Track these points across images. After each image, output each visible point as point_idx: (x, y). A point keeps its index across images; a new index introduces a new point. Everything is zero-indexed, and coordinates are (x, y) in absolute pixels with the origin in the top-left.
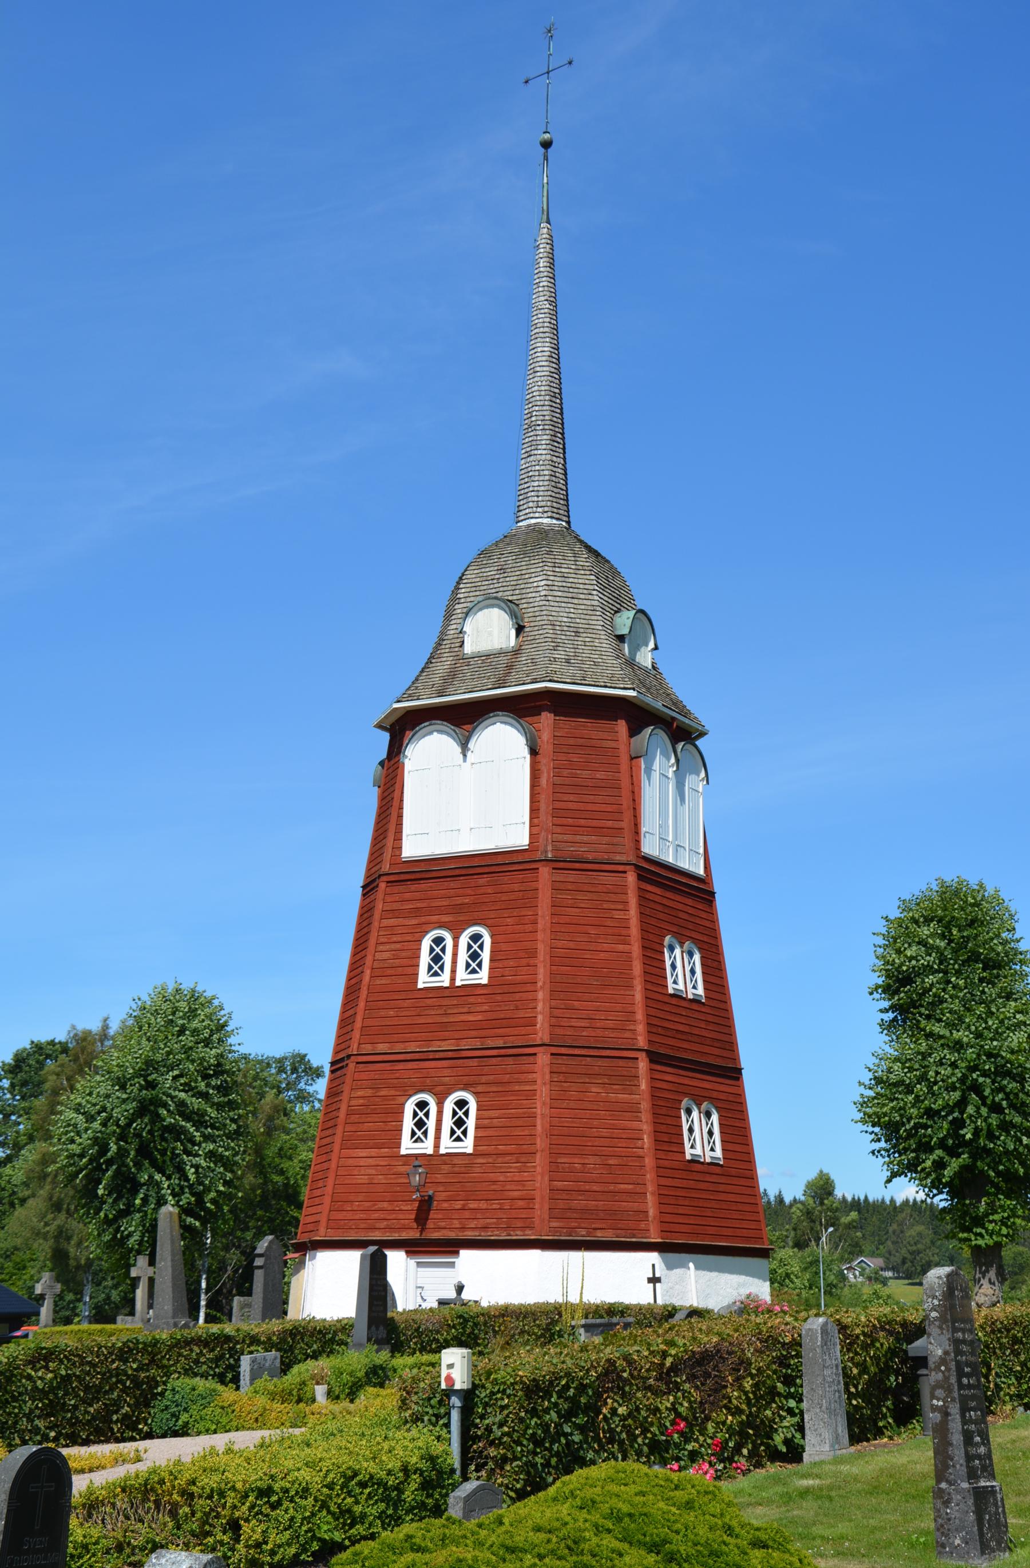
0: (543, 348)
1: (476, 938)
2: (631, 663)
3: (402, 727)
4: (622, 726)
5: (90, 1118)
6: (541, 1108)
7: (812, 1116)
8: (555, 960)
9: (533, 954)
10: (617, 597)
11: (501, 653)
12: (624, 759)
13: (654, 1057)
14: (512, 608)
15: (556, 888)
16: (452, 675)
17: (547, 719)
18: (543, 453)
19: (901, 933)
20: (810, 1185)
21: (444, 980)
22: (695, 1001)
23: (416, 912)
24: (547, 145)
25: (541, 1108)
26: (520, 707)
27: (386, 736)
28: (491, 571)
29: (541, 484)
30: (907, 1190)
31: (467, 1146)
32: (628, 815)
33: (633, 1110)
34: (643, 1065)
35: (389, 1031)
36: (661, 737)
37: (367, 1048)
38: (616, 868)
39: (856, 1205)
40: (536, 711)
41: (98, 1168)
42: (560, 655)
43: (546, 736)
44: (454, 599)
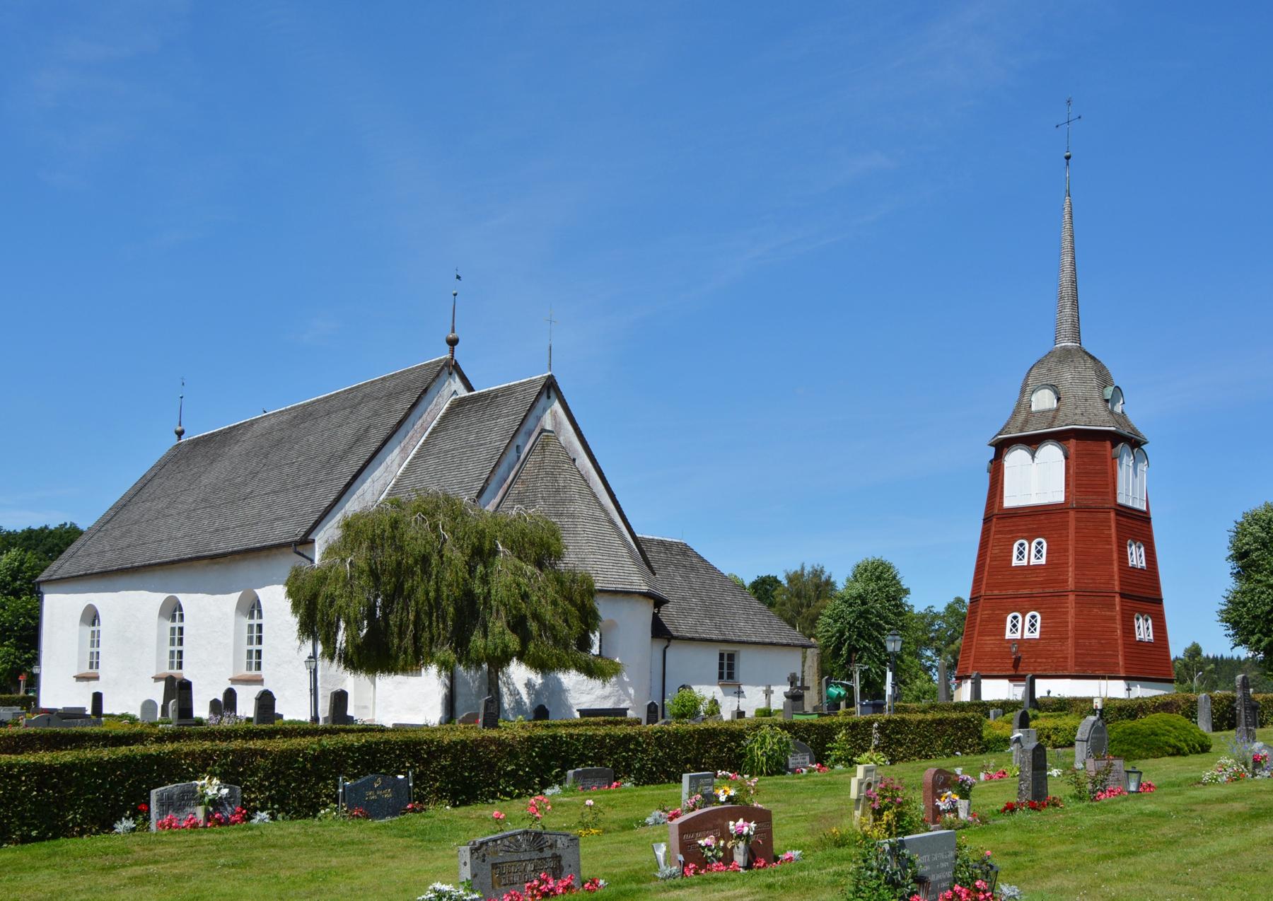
0: (1067, 259)
1: (1039, 543)
2: (1112, 412)
3: (1002, 447)
4: (1108, 444)
5: (836, 621)
6: (1071, 618)
7: (1196, 618)
8: (1076, 553)
9: (1067, 550)
10: (1104, 377)
11: (1049, 410)
12: (1109, 459)
13: (1122, 595)
14: (1054, 388)
15: (1077, 520)
16: (1026, 422)
17: (1072, 442)
18: (1068, 311)
19: (1241, 531)
20: (1186, 650)
21: (1025, 562)
22: (1142, 569)
23: (1011, 532)
24: (1068, 158)
25: (1071, 618)
26: (1059, 438)
27: (993, 449)
28: (1044, 371)
29: (1067, 326)
30: (1243, 653)
31: (1037, 635)
32: (1111, 486)
33: (1113, 619)
34: (1117, 599)
35: (996, 585)
36: (1128, 447)
37: (989, 593)
38: (1106, 511)
39: (1215, 660)
40: (1068, 439)
41: (840, 643)
42: (1078, 411)
43: (1072, 450)
44: (1025, 385)
